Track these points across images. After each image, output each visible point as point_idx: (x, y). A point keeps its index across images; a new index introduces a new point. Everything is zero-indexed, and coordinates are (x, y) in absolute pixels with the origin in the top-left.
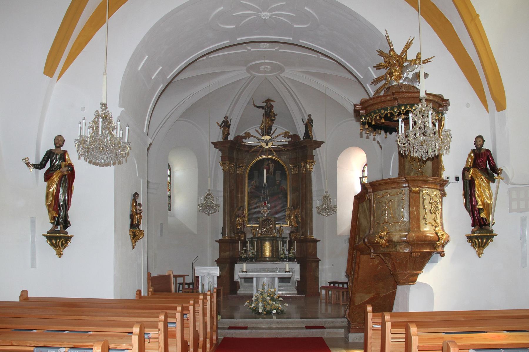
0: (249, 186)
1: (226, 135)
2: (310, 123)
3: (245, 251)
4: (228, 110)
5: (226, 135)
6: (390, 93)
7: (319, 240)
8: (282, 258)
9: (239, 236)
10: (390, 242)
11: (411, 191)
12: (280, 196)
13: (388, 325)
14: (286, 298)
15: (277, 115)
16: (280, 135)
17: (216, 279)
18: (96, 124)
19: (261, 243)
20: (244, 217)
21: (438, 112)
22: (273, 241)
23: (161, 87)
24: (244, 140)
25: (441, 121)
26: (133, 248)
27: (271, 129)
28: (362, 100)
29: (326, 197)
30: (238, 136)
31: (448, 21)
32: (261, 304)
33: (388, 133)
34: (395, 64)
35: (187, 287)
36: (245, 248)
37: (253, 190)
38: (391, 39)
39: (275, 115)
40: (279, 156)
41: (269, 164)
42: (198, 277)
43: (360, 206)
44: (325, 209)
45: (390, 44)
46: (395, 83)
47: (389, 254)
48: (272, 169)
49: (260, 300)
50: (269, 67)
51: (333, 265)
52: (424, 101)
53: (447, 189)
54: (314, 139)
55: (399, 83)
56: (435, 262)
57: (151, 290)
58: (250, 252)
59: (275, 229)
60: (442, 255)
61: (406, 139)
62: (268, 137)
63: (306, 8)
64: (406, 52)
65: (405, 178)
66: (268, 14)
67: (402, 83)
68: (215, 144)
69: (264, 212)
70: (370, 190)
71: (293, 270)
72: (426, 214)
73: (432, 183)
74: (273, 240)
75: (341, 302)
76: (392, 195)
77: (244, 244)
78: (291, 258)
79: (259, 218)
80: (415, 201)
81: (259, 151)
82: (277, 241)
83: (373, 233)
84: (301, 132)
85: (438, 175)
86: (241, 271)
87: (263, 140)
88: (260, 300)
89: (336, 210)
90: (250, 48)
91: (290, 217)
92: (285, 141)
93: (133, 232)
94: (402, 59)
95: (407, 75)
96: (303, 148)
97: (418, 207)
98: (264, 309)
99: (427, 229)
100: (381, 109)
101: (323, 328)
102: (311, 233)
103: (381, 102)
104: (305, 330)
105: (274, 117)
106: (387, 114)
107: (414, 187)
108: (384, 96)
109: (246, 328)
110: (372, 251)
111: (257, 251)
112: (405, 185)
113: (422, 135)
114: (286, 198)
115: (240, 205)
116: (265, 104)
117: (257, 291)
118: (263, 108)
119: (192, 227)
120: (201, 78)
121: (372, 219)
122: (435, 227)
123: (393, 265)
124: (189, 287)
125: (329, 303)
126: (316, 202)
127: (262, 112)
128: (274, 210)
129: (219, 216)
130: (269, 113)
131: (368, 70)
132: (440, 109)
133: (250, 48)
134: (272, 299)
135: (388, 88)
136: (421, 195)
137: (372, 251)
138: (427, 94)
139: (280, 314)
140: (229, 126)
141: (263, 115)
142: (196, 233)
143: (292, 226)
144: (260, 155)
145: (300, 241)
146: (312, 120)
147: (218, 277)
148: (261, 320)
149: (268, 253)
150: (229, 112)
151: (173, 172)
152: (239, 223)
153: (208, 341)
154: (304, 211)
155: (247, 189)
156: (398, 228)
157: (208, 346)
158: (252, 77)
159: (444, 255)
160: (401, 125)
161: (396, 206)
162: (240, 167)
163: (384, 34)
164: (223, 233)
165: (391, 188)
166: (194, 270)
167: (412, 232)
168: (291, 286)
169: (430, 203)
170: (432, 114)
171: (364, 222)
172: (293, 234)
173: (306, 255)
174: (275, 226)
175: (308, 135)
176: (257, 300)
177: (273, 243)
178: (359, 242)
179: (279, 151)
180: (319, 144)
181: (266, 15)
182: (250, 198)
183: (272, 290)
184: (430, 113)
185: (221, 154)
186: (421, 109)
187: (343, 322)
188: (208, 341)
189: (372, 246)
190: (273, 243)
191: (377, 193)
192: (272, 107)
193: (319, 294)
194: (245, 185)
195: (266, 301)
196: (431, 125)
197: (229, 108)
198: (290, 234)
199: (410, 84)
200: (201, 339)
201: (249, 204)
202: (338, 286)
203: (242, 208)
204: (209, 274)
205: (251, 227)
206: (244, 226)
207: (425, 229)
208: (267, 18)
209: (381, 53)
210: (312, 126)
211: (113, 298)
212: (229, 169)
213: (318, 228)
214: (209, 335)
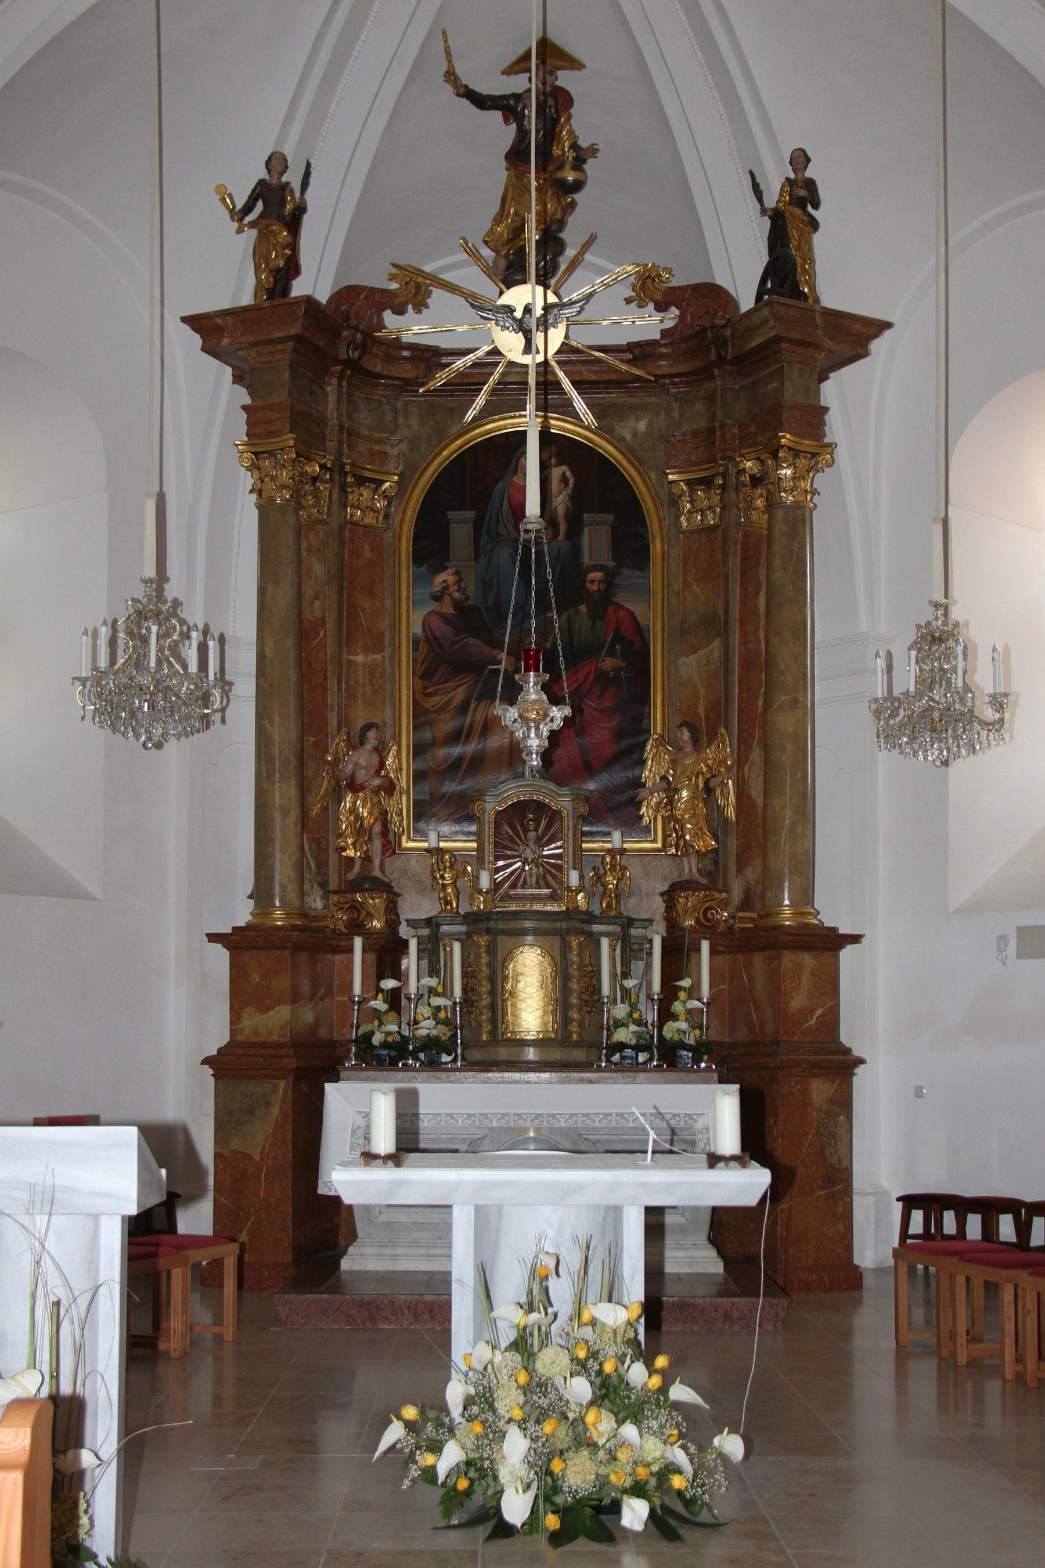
2: (801, 203)
3: (394, 998)
7: (856, 939)
8: (621, 1046)
9: (355, 907)
15: (593, 151)
22: (569, 937)
32: (515, 1447)
36: (389, 984)
49: (509, 1401)
51: (918, 1093)
58: (424, 1011)
74: (563, 935)
77: (387, 955)
87: (509, 310)
88: (509, 1401)
91: (671, 790)
98: (548, 1489)
102: (806, 895)
105: (579, 164)
111: (468, 1002)
118: (509, 107)
140: (294, 223)
141: (517, 156)
146: (811, 185)
149: (530, 1012)
152: (361, 831)
154: (756, 755)
162: (361, 481)
172: (687, 901)
174: (578, 850)
175: (786, 269)
176: (482, 1400)
177: (565, 949)
190: (565, 949)
206: (391, 847)
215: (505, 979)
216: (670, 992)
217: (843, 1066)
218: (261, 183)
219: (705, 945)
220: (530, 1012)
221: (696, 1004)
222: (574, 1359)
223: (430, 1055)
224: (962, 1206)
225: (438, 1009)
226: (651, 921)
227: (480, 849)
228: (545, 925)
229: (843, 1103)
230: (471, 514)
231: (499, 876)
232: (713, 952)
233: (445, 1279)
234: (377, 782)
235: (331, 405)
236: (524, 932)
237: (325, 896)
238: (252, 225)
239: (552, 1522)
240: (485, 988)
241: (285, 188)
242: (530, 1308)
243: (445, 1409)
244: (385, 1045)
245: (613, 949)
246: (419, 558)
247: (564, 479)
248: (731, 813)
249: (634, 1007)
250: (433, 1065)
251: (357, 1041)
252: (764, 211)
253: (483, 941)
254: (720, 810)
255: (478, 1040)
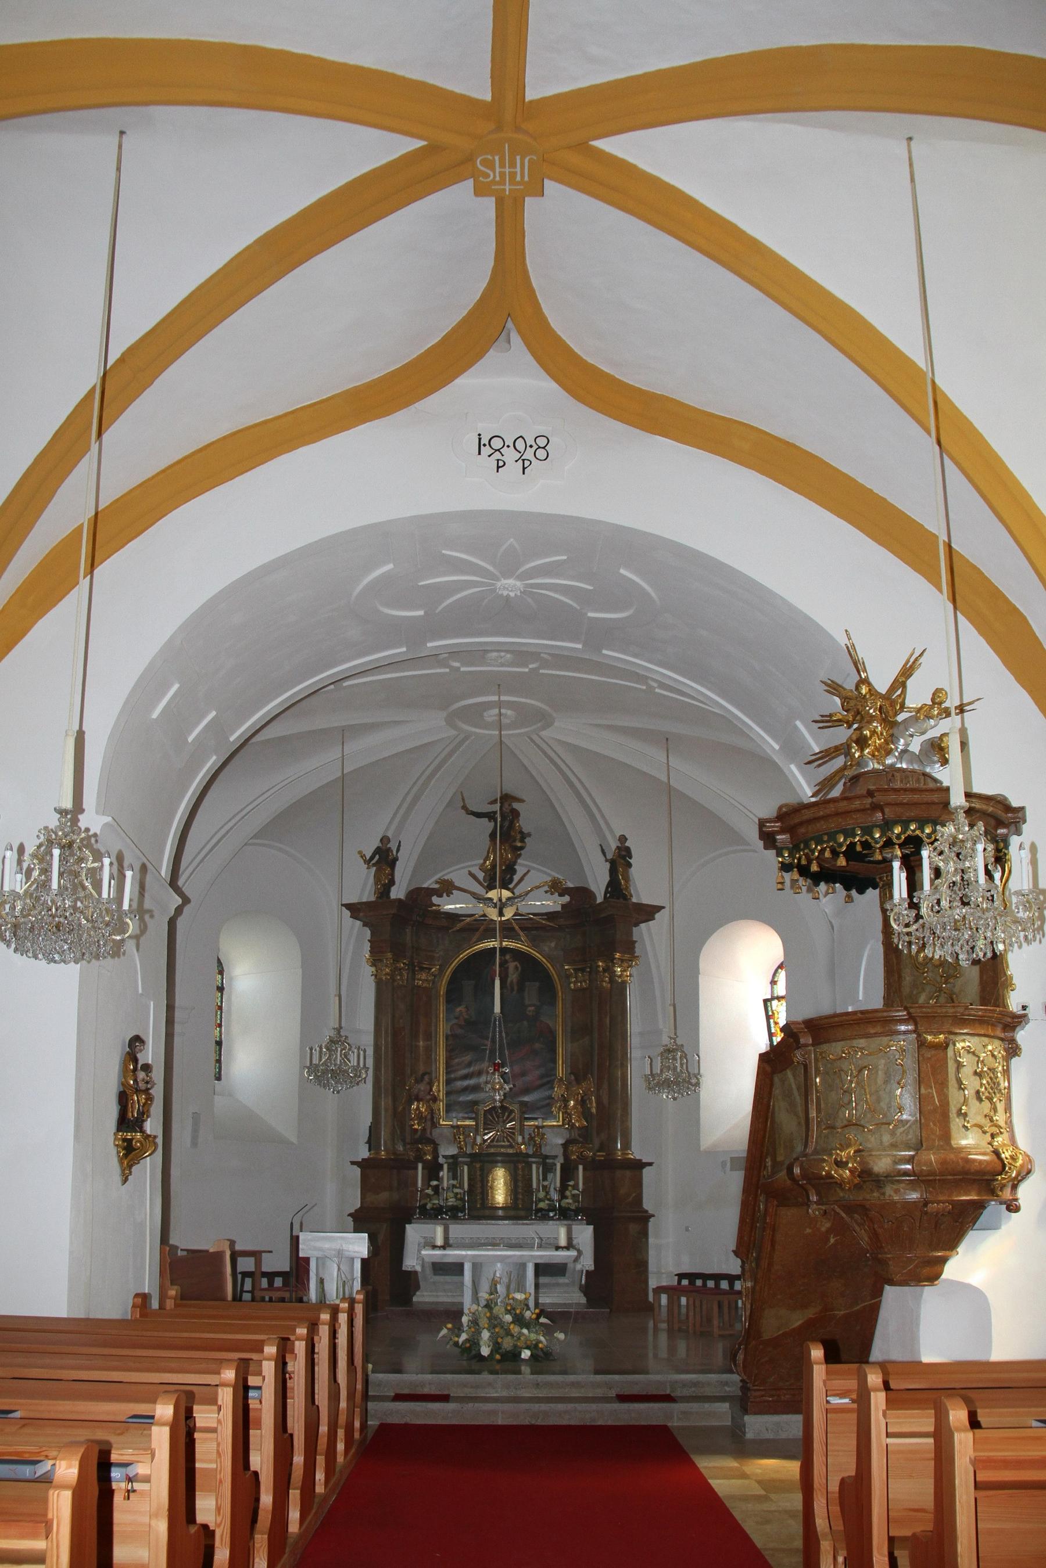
0: (448, 1020)
1: (384, 887)
2: (624, 858)
3: (436, 1189)
4: (393, 819)
5: (384, 887)
6: (861, 789)
7: (650, 1164)
8: (541, 1210)
9: (418, 1149)
10: (866, 1177)
11: (922, 1044)
12: (537, 1046)
13: (878, 1399)
14: (558, 1318)
15: (529, 835)
16: (537, 887)
17: (358, 1265)
18: (41, 861)
19: (482, 1169)
20: (435, 1099)
21: (994, 840)
22: (517, 1165)
23: (212, 762)
24: (435, 899)
25: (1000, 858)
26: (125, 1181)
27: (514, 872)
28: (780, 808)
29: (669, 1051)
30: (418, 890)
31: (1016, 610)
32: (486, 1335)
33: (854, 892)
34: (872, 716)
35: (264, 1283)
36: (435, 1183)
37: (459, 1031)
38: (861, 654)
39: (523, 836)
40: (534, 942)
41: (506, 962)
42: (307, 1260)
43: (776, 1079)
44: (667, 1084)
45: (858, 665)
46: (872, 765)
47: (863, 1206)
48: (513, 977)
49: (484, 1322)
50: (509, 712)
51: (687, 1229)
52: (961, 817)
53: (1021, 1036)
54: (634, 900)
55: (883, 764)
56: (994, 1227)
57: (172, 1293)
58: (451, 1194)
59: (522, 1133)
60: (1013, 1207)
61: (913, 913)
62: (506, 894)
63: (622, 571)
64: (904, 685)
65: (906, 1009)
66: (518, 583)
67: (892, 766)
68: (355, 910)
69: (494, 1089)
70: (806, 1039)
71: (576, 1243)
72: (965, 1102)
73: (981, 1021)
75: (716, 1330)
76: (870, 1054)
77: (433, 1170)
78: (569, 1209)
79: (476, 1103)
80: (933, 1068)
81: (481, 927)
82: (529, 1165)
83: (816, 1152)
84: (598, 882)
85: (997, 999)
86: (422, 1244)
87: (491, 899)
88: (484, 1322)
89: (698, 1084)
90: (457, 664)
91: (566, 1101)
92: (551, 903)
93: (124, 1140)
94: (893, 704)
95: (907, 745)
96: (603, 923)
97: (943, 1085)
98: (496, 1347)
99: (970, 1142)
100: (837, 832)
101: (668, 1398)
102: (627, 1145)
103: (837, 814)
104: (617, 1406)
105: (522, 840)
106: (852, 845)
107: (930, 1033)
108: (843, 798)
109: (445, 1398)
110: (814, 1198)
111: (471, 1191)
112: (903, 1028)
113: (957, 903)
114: (553, 1050)
115: (421, 1068)
116: (497, 807)
117: (476, 1299)
118: (490, 816)
119: (284, 1123)
120: (318, 738)
121: (813, 1114)
122: (993, 1136)
123: (875, 1236)
124: (271, 1283)
125: (680, 1330)
126: (638, 1065)
127: (487, 826)
128: (519, 1083)
129: (362, 1099)
130: (507, 829)
131: (796, 727)
132: (1001, 831)
133: (457, 664)
134: (519, 1320)
135: (855, 779)
136: (950, 1052)
137: (814, 1198)
138: (968, 795)
139: (542, 1359)
140: (393, 863)
141: (493, 836)
142: (294, 1140)
143: (573, 1126)
144: (480, 940)
145: (592, 1166)
146: (628, 850)
147: (363, 1260)
148: (486, 1377)
149: (500, 1196)
150: (393, 827)
151: (231, 979)
152: (420, 1117)
153: (341, 1433)
154: (605, 1086)
155: (442, 1028)
156: (886, 1139)
157: (341, 1446)
158: (462, 736)
159: (1017, 1209)
160: (899, 878)
161: (880, 1081)
162: (422, 969)
163: (843, 641)
164: (372, 1142)
165: (867, 1036)
166: (295, 1241)
167: (928, 1149)
168: (567, 1285)
169: (975, 1073)
170: (985, 849)
171: (787, 1122)
172: (573, 1148)
173: (611, 1199)
174: (522, 1126)
175: (617, 888)
176: (475, 1322)
177: (516, 1169)
178: (773, 1173)
179: (536, 929)
180: (649, 912)
181: (510, 586)
182: (451, 1052)
183: (519, 1296)
184: (980, 847)
185: (368, 933)
186: (955, 838)
187: (726, 1384)
188: (341, 1433)
189: (814, 1186)
190: (516, 1169)
191: (825, 1047)
192: (516, 814)
193: (649, 1309)
194: (437, 1017)
195: (501, 1324)
196: (982, 878)
197: (395, 814)
198: (565, 1146)
199: (916, 767)
200: (324, 1429)
201: (448, 1066)
202: (717, 1285)
203: (427, 1077)
204: (340, 1253)
205: (452, 1126)
206: (435, 1125)
207: (964, 1142)
208: (512, 594)
209: (834, 688)
210: (630, 865)
211: (63, 1314)
212: (392, 975)
213: (646, 1127)
214: (342, 1419)
215: (488, 1181)
216: (564, 1187)
217: (644, 1218)
218: (378, 848)
219: (581, 1167)
220: (500, 1196)
221: (576, 1192)
222: (506, 1309)
223: (454, 1213)
224: (705, 1277)
225: (457, 1194)
226: (556, 1157)
227: (477, 1125)
228: (507, 1159)
229: (645, 1233)
230: (473, 982)
231: (486, 1137)
232: (584, 1169)
233: (462, 1304)
234: (428, 1097)
235: (408, 938)
236: (497, 1162)
237: (404, 1145)
238: (374, 865)
239: (498, 1357)
240: (479, 1185)
241: (389, 850)
242: (491, 1294)
243: (462, 1325)
244: (432, 1209)
245: (538, 1169)
246: (449, 1000)
247: (516, 968)
248: (594, 1110)
249: (547, 1193)
250: (455, 1218)
251: (419, 1207)
252: (607, 861)
253: (478, 1165)
254: (589, 1109)
255: (476, 1206)
